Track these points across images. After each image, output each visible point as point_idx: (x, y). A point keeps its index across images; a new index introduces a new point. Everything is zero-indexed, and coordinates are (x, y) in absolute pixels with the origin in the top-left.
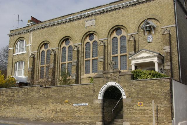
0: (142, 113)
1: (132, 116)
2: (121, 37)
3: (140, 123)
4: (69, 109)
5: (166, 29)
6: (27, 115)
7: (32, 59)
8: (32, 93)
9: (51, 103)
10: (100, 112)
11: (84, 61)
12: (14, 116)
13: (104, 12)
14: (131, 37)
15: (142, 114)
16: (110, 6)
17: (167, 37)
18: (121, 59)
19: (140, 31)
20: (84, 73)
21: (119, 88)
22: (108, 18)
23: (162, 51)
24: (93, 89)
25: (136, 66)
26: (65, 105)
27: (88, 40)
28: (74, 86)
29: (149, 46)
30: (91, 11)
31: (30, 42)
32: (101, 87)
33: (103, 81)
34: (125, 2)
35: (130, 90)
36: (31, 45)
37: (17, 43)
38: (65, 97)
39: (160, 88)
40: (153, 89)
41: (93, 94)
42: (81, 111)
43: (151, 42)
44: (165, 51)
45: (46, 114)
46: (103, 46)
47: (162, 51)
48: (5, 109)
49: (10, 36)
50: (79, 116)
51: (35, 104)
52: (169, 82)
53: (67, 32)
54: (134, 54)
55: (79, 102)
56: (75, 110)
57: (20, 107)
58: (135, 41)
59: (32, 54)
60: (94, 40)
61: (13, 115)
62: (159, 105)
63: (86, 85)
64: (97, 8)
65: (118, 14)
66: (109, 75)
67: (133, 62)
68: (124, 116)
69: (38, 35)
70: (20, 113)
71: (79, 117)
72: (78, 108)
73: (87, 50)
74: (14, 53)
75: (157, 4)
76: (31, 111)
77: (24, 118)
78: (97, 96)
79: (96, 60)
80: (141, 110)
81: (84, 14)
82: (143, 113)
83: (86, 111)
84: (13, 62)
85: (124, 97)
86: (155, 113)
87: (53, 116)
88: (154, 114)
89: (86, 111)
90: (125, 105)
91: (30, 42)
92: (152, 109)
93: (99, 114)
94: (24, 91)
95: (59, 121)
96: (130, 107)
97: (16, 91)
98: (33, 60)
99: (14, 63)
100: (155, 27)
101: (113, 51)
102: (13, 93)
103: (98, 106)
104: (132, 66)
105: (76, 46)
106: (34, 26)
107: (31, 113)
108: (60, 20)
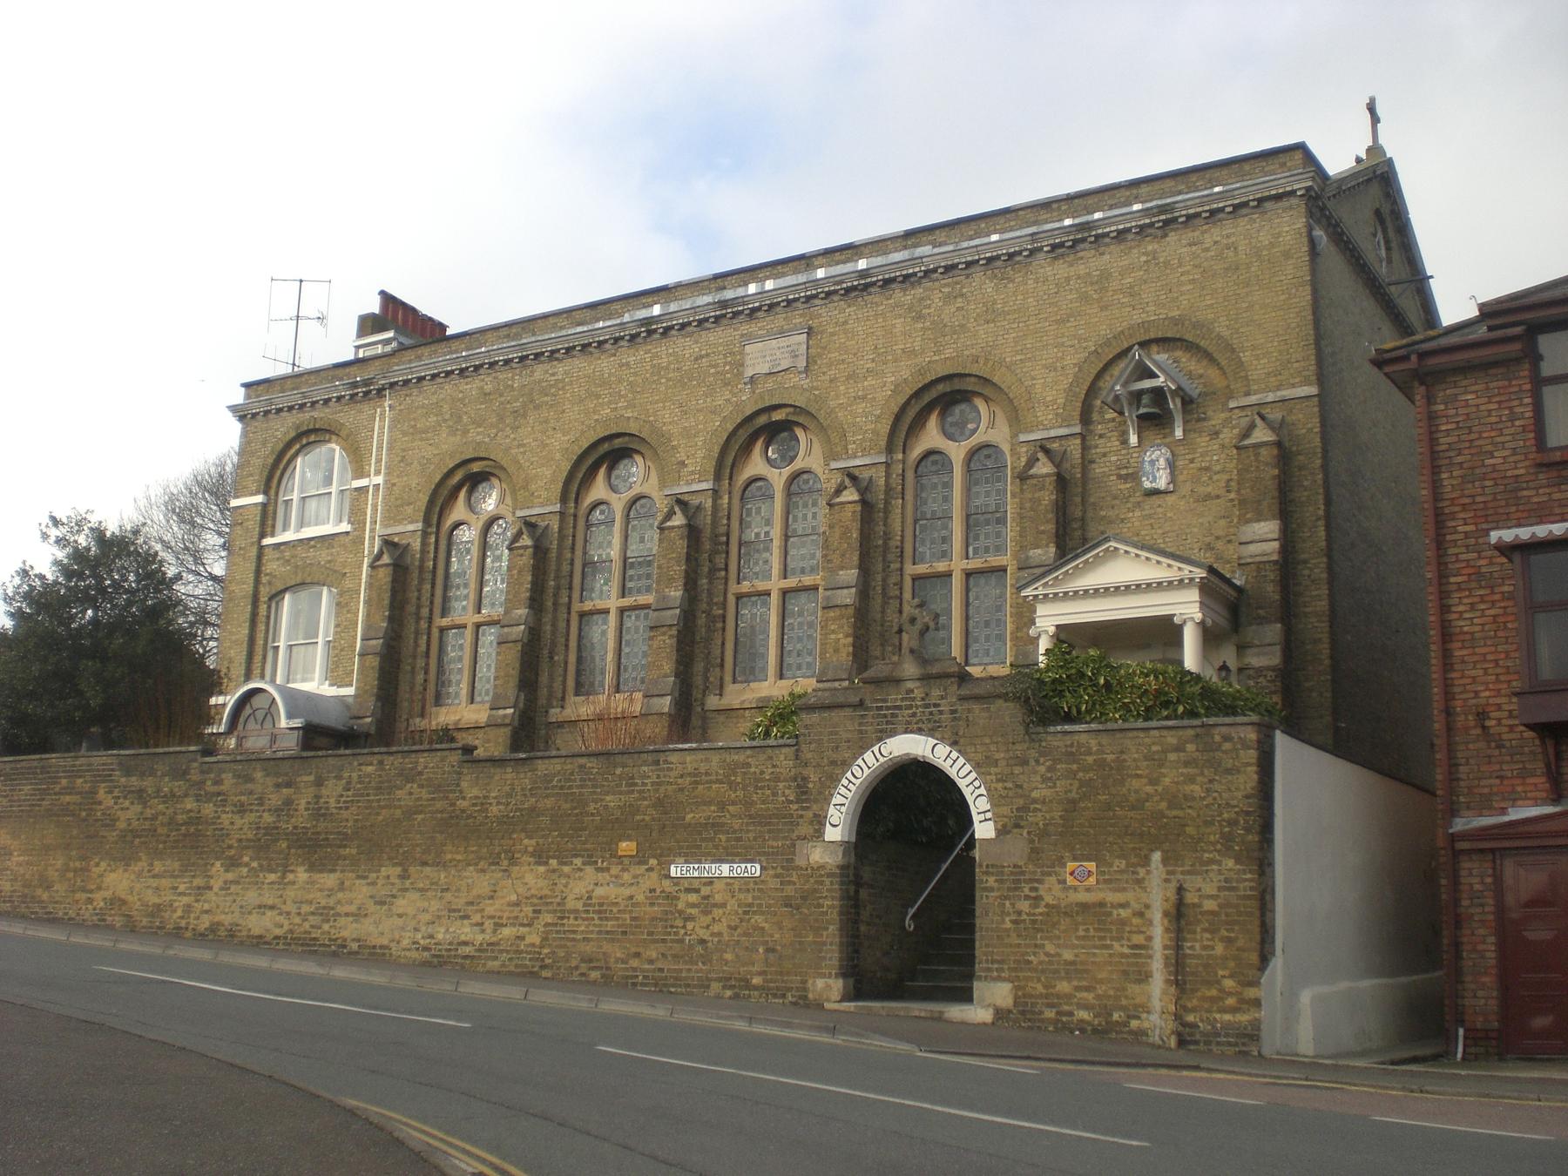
0: (1087, 930)
1: (1027, 946)
2: (973, 453)
3: (1077, 989)
4: (640, 898)
5: (1260, 410)
6: (372, 928)
7: (385, 576)
8: (406, 795)
11: (731, 599)
12: (291, 931)
13: (866, 287)
14: (1041, 455)
15: (1092, 933)
16: (905, 248)
17: (1267, 464)
18: (967, 590)
19: (1095, 416)
20: (728, 678)
21: (952, 773)
22: (894, 326)
23: (1231, 547)
24: (795, 779)
25: (1067, 636)
26: (615, 870)
28: (673, 758)
29: (1150, 516)
30: (783, 275)
31: (379, 461)
32: (846, 765)
35: (1021, 787)
36: (379, 480)
38: (618, 825)
39: (1199, 779)
41: (795, 807)
42: (717, 912)
43: (1166, 492)
45: (498, 926)
46: (858, 508)
47: (1231, 552)
48: (233, 888)
49: (242, 418)
50: (703, 942)
51: (425, 864)
52: (1249, 748)
53: (626, 408)
54: (1056, 568)
56: (681, 905)
57: (330, 880)
58: (1062, 482)
59: (388, 543)
62: (1192, 883)
63: (749, 752)
64: (820, 260)
65: (959, 302)
66: (894, 697)
67: (1048, 619)
70: (327, 913)
71: (706, 949)
72: (697, 891)
75: (1207, 250)
76: (401, 904)
77: (355, 946)
78: (820, 821)
79: (993, 580)
80: (1084, 907)
81: (740, 292)
84: (262, 589)
85: (984, 830)
86: (1167, 930)
89: (748, 909)
91: (379, 461)
92: (1147, 907)
93: (831, 927)
94: (355, 775)
95: (577, 968)
96: (1016, 889)
97: (306, 778)
98: (394, 581)
99: (264, 599)
100: (1195, 394)
103: (822, 883)
104: (1038, 638)
105: (679, 502)
106: (410, 355)
107: (400, 916)
108: (579, 324)
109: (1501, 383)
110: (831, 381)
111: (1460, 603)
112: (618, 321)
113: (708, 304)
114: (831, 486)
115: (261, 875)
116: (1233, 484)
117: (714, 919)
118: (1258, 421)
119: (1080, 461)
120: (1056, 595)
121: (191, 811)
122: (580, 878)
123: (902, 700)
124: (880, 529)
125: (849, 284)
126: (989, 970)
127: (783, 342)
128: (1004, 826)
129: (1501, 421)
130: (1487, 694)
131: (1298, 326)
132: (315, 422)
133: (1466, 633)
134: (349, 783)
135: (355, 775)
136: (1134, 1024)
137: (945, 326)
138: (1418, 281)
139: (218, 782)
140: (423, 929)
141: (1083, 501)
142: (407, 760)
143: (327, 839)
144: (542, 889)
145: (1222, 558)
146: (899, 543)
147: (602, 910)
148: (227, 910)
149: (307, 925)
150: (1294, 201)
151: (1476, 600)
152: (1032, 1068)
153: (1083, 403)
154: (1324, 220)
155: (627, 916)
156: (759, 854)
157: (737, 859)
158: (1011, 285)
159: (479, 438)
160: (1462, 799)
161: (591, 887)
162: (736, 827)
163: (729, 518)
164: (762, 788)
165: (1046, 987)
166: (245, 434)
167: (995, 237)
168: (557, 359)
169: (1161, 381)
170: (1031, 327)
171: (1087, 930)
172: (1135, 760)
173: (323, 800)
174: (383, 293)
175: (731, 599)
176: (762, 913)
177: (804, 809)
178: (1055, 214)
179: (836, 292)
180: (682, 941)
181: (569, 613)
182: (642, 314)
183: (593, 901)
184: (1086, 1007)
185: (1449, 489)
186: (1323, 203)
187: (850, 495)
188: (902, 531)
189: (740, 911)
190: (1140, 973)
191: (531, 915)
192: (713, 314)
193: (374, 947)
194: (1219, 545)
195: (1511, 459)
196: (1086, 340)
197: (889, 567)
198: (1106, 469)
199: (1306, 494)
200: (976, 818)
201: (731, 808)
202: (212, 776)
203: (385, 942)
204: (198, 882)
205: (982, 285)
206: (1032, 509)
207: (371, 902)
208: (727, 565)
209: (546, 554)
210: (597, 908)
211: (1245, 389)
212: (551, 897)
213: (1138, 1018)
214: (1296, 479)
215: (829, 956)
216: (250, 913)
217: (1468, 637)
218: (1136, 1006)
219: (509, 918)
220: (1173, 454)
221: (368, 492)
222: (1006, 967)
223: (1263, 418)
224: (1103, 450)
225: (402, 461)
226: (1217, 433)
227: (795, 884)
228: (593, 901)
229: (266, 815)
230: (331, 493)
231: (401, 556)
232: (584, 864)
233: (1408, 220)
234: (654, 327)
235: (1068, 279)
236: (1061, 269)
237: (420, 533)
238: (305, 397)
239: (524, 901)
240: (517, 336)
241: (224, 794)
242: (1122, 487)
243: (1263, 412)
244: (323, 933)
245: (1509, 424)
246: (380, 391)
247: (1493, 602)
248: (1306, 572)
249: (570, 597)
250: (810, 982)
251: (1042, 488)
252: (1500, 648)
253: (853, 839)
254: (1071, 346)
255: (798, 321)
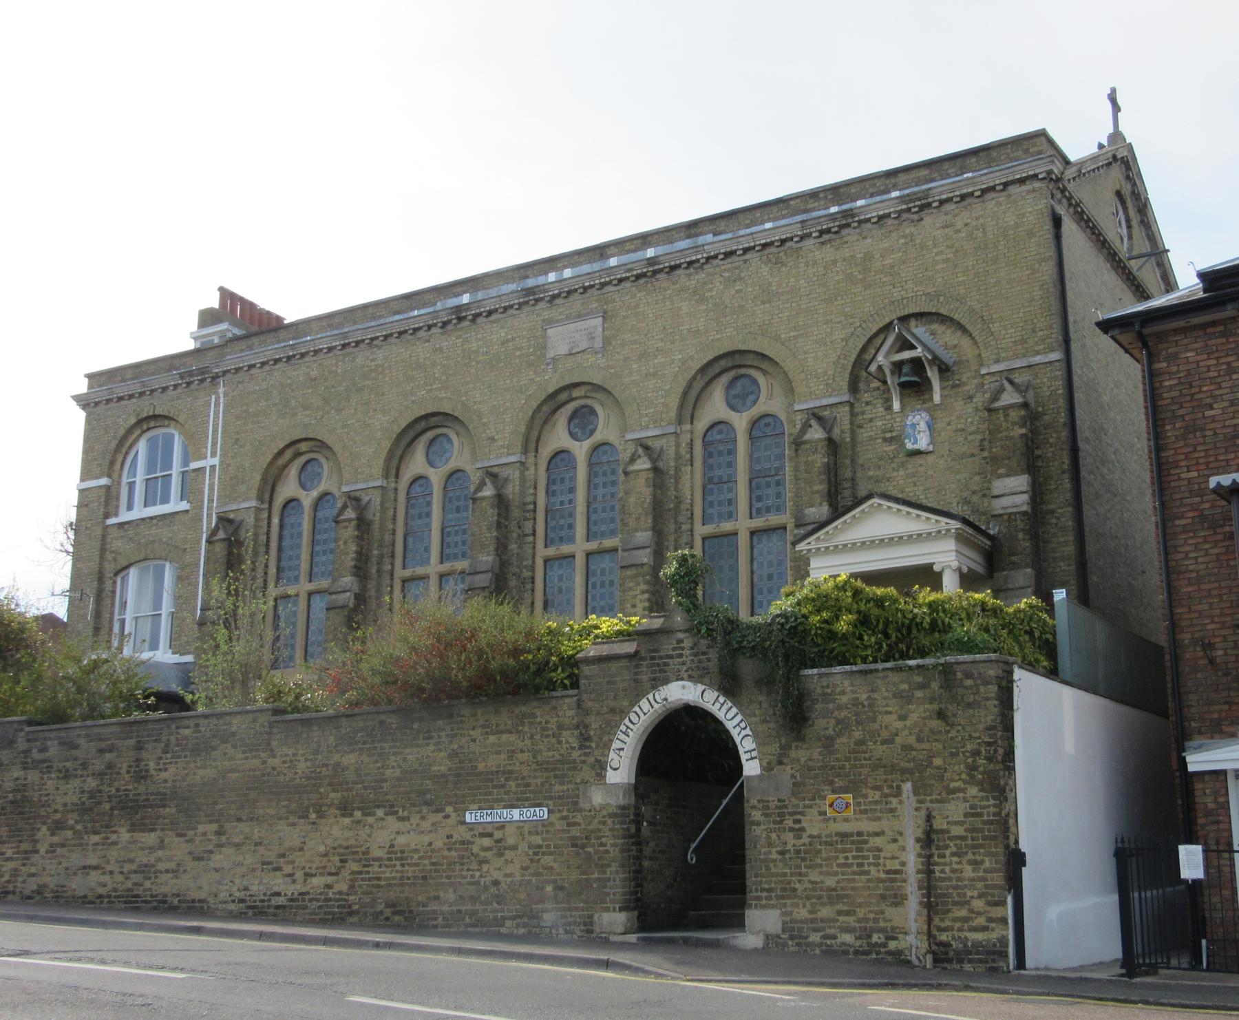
2: (754, 423)
3: (840, 913)
5: (1009, 376)
9: (333, 811)
10: (615, 853)
11: (539, 562)
12: (115, 890)
13: (655, 273)
14: (813, 422)
16: (688, 237)
17: (1015, 423)
19: (862, 386)
22: (680, 308)
23: (986, 501)
24: (577, 727)
26: (415, 820)
27: (559, 437)
29: (913, 475)
30: (580, 264)
31: (214, 444)
32: (623, 713)
33: (636, 681)
34: (778, 219)
36: (216, 461)
37: (127, 453)
40: (908, 723)
42: (509, 854)
44: (999, 506)
48: (59, 851)
49: (85, 406)
50: (496, 883)
51: (239, 820)
55: (496, 801)
57: (150, 838)
58: (832, 445)
60: (598, 436)
61: (105, 885)
68: (748, 875)
69: (263, 403)
70: (146, 870)
72: (490, 835)
73: (711, 468)
74: (112, 509)
75: (958, 231)
76: (218, 859)
78: (600, 767)
80: (844, 836)
81: (541, 280)
82: (854, 857)
83: (536, 854)
84: (107, 565)
85: (751, 768)
87: (344, 888)
88: (912, 859)
90: (756, 815)
91: (214, 444)
95: (381, 912)
100: (950, 362)
101: (706, 504)
102: (108, 755)
107: (216, 870)
109: (1219, 341)
110: (625, 360)
111: (1185, 543)
112: (431, 310)
113: (513, 292)
114: (626, 456)
115: (86, 837)
116: (986, 443)
117: (506, 860)
118: (1007, 385)
119: (848, 426)
120: (827, 548)
121: (17, 779)
122: (382, 828)
123: (674, 649)
124: (672, 493)
125: (639, 271)
126: (759, 898)
127: (582, 325)
128: (769, 763)
129: (1220, 376)
130: (1213, 626)
131: (1042, 298)
132: (154, 408)
133: (1192, 571)
134: (167, 746)
135: (173, 739)
136: (893, 945)
137: (726, 307)
138: (1158, 254)
139: (43, 750)
140: (237, 881)
141: (853, 462)
142: (221, 722)
143: (148, 800)
144: (348, 839)
145: (978, 511)
146: (689, 506)
147: (396, 854)
148: (53, 873)
149: (129, 884)
150: (1037, 185)
151: (1200, 540)
152: (789, 994)
153: (851, 374)
154: (1064, 201)
155: (427, 862)
156: (546, 798)
157: (526, 804)
158: (784, 269)
159: (306, 420)
160: (1193, 724)
161: (394, 835)
162: (525, 774)
163: (535, 488)
164: (547, 736)
165: (811, 912)
166: (88, 421)
167: (768, 225)
168: (376, 346)
169: (918, 352)
170: (804, 306)
171: (847, 858)
172: (885, 698)
173: (143, 763)
174: (222, 290)
175: (539, 562)
176: (550, 854)
177: (586, 755)
178: (822, 202)
179: (627, 278)
180: (478, 883)
181: (392, 579)
182: (452, 302)
183: (396, 849)
184: (848, 930)
185: (1173, 439)
186: (1064, 186)
187: (643, 464)
188: (692, 495)
189: (531, 852)
190: (895, 896)
191: (339, 864)
192: (517, 301)
193: (193, 901)
194: (975, 499)
195: (1230, 410)
196: (852, 317)
197: (680, 528)
198: (872, 433)
199: (1051, 449)
200: (744, 757)
201: (519, 756)
202: (38, 744)
203: (202, 895)
204: (25, 846)
205: (758, 267)
206: (806, 472)
207: (189, 858)
208: (534, 531)
209: (369, 525)
210: (399, 855)
211: (994, 357)
212: (356, 847)
213: (895, 938)
214: (1042, 437)
215: (612, 891)
216: (75, 874)
217: (1194, 575)
218: (893, 929)
219: (317, 868)
220: (932, 417)
221: (205, 472)
222: (773, 895)
223: (1011, 382)
224: (869, 416)
225: (236, 443)
226: (971, 398)
227: (579, 824)
228: (396, 849)
229: (90, 779)
230: (171, 475)
231: (236, 532)
232: (387, 814)
233: (1147, 199)
234: (464, 314)
235: (835, 262)
236: (827, 253)
237: (253, 509)
238: (144, 386)
239: (332, 851)
240: (340, 326)
241: (50, 761)
242: (887, 449)
243: (1011, 377)
244: (145, 890)
245: (1228, 378)
246: (215, 378)
247: (1216, 542)
248: (1054, 521)
249: (392, 565)
250: (596, 917)
251: (815, 452)
252: (1223, 584)
253: (633, 781)
254: (840, 322)
255: (594, 306)
